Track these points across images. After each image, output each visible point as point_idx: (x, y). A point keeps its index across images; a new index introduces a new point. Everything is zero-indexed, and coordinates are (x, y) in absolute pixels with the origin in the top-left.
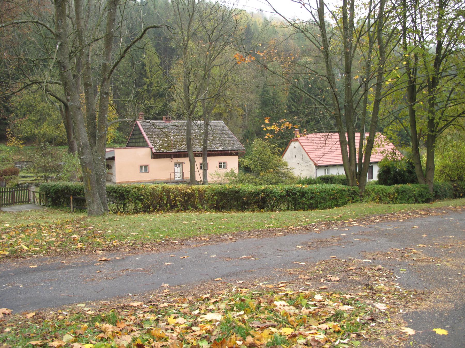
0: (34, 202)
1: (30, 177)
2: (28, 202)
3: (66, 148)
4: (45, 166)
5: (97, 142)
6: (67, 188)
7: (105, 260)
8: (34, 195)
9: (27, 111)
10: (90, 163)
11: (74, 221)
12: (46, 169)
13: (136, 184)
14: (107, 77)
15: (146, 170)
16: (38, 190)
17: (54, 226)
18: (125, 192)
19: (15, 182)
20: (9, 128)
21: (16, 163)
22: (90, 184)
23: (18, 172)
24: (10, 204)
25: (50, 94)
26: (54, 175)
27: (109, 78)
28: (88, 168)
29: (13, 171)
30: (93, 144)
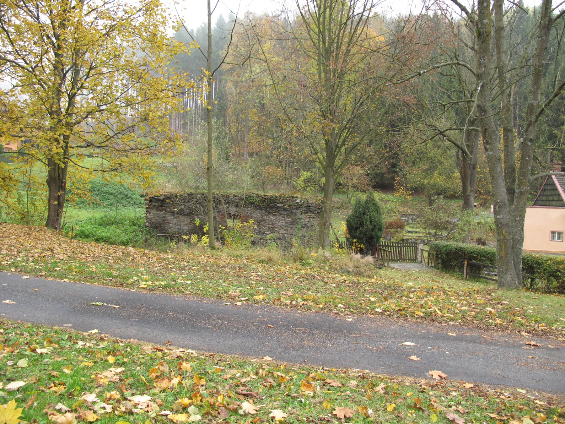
0: (421, 262)
1: (416, 232)
2: (415, 260)
3: (461, 203)
4: (436, 222)
5: (515, 200)
6: (462, 250)
7: (534, 345)
8: (422, 254)
9: (418, 158)
10: (507, 225)
11: (483, 291)
12: (436, 226)
13: (551, 256)
14: (533, 120)
15: (559, 238)
16: (427, 248)
17: (461, 293)
18: (535, 263)
19: (401, 236)
20: (398, 177)
21: (402, 216)
22: (505, 249)
23: (404, 226)
24: (397, 261)
25: (448, 140)
26: (444, 234)
27: (536, 121)
28: (504, 231)
29: (399, 224)
30: (511, 202)
